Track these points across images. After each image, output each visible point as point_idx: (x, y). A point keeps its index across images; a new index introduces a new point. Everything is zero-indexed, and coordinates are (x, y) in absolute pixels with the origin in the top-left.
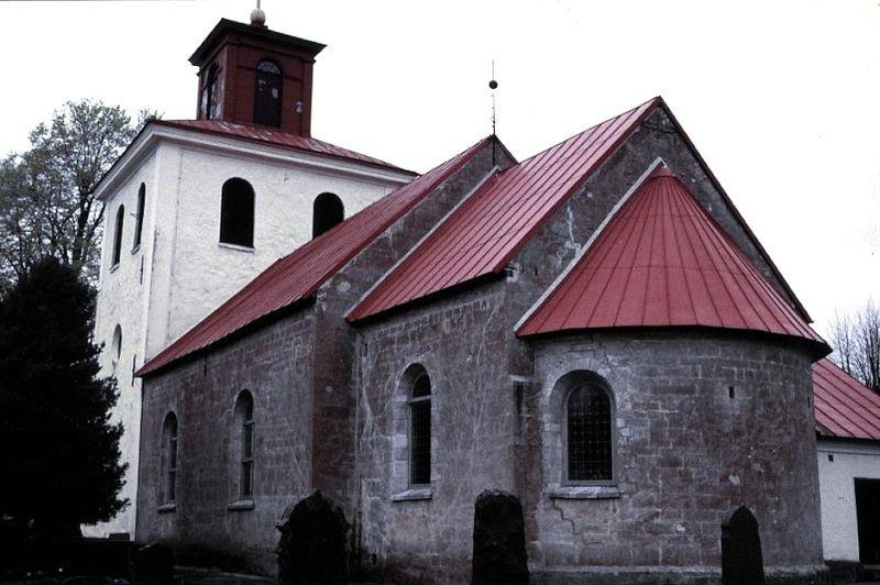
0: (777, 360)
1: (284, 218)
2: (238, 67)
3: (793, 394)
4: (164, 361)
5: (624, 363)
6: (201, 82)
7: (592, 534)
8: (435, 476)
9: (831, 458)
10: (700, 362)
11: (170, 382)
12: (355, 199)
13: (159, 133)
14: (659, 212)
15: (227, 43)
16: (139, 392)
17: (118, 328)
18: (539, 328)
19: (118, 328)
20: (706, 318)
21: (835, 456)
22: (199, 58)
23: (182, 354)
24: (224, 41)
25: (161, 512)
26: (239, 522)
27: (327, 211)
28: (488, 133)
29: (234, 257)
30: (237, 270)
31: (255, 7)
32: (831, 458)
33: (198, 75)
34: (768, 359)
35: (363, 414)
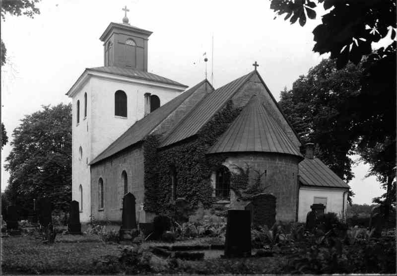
1: (137, 108)
2: (118, 43)
4: (97, 160)
6: (105, 48)
8: (104, 206)
10: (257, 163)
11: (101, 169)
12: (165, 98)
13: (90, 73)
14: (240, 123)
15: (114, 33)
16: (90, 170)
17: (81, 185)
18: (224, 149)
19: (81, 185)
20: (258, 148)
22: (104, 38)
23: (106, 157)
24: (112, 32)
25: (99, 211)
26: (41, 153)
27: (154, 101)
28: (205, 79)
29: (120, 120)
30: (121, 126)
31: (124, 16)
33: (104, 45)
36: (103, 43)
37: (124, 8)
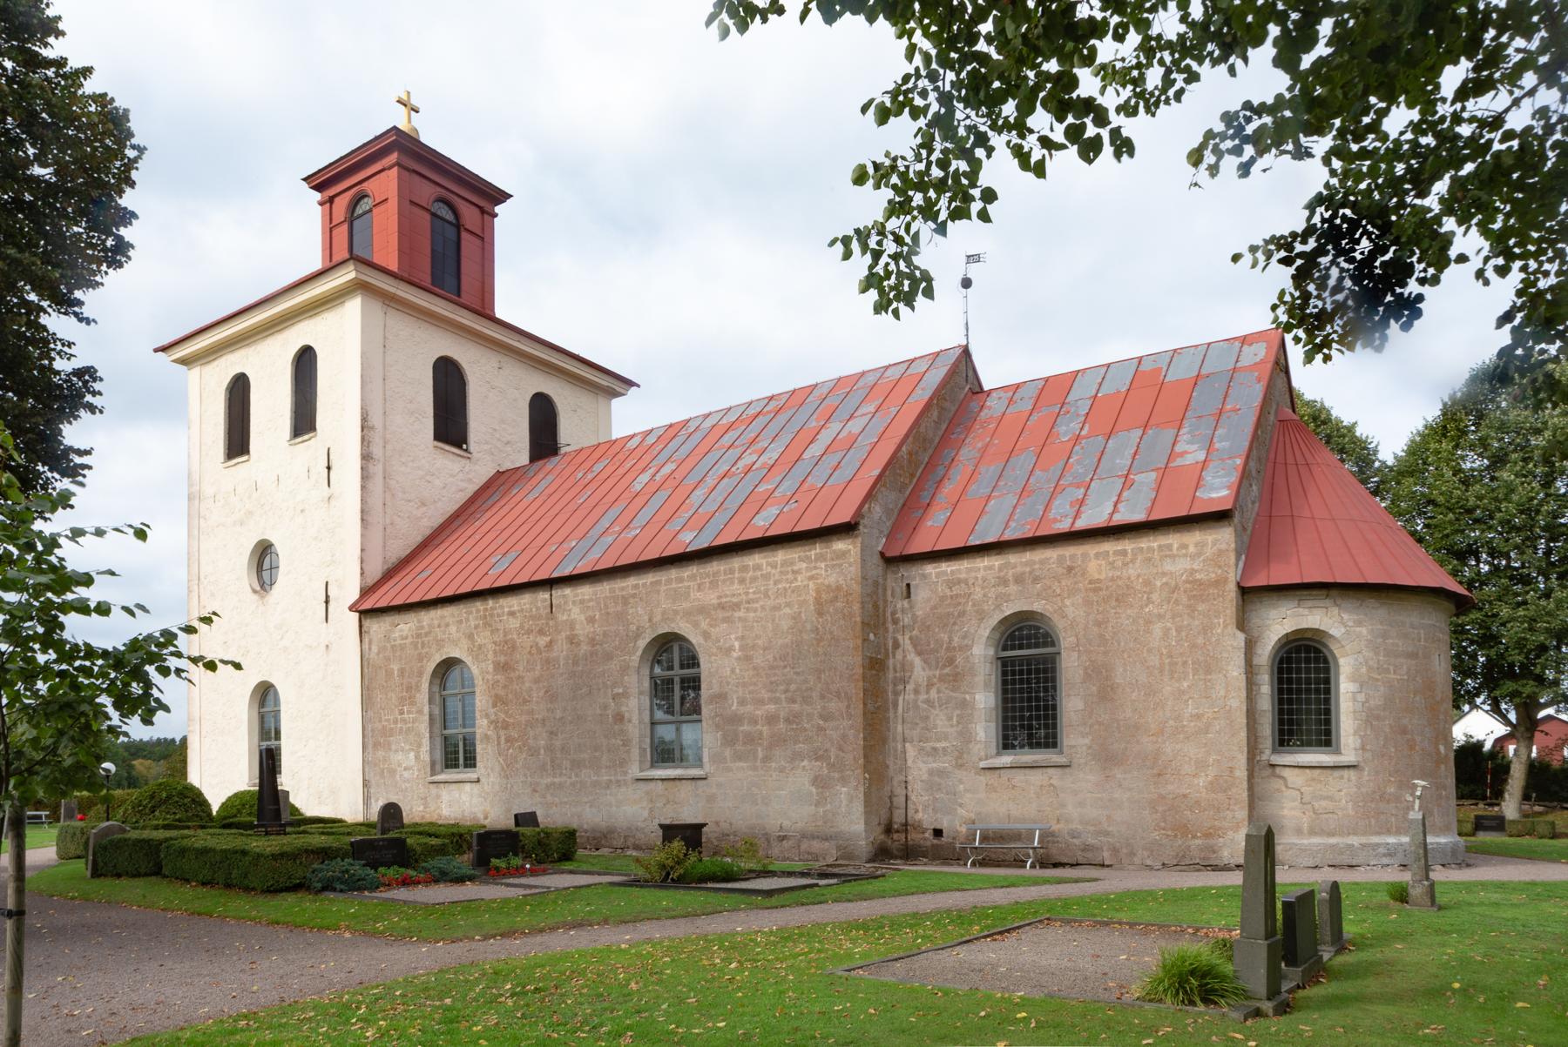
5: (1359, 623)
7: (1324, 803)
30: (448, 478)
35: (906, 667)
36: (317, 196)
37: (405, 97)
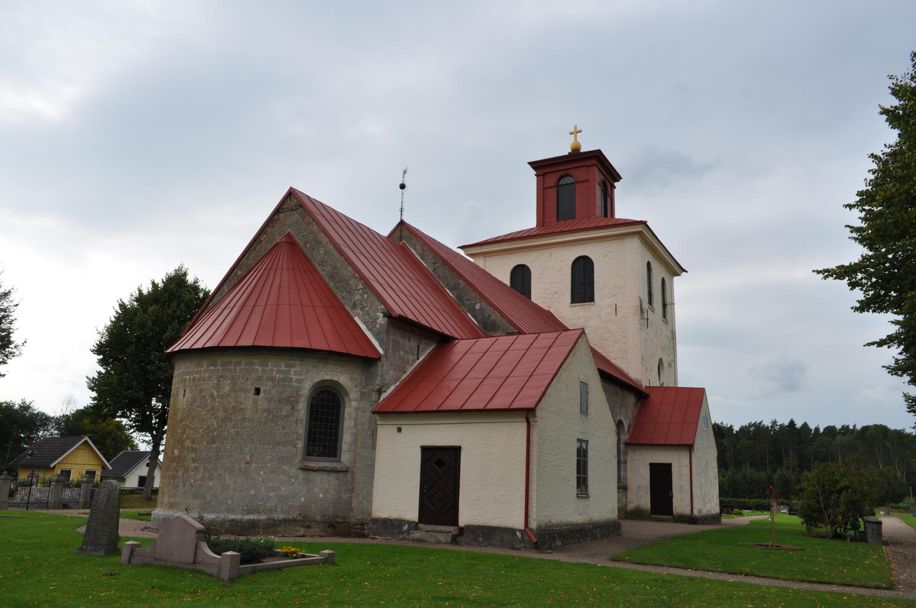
0: (215, 365)
3: (227, 388)
9: (399, 430)
21: (404, 428)
32: (399, 430)
34: (208, 366)
37: (573, 130)
